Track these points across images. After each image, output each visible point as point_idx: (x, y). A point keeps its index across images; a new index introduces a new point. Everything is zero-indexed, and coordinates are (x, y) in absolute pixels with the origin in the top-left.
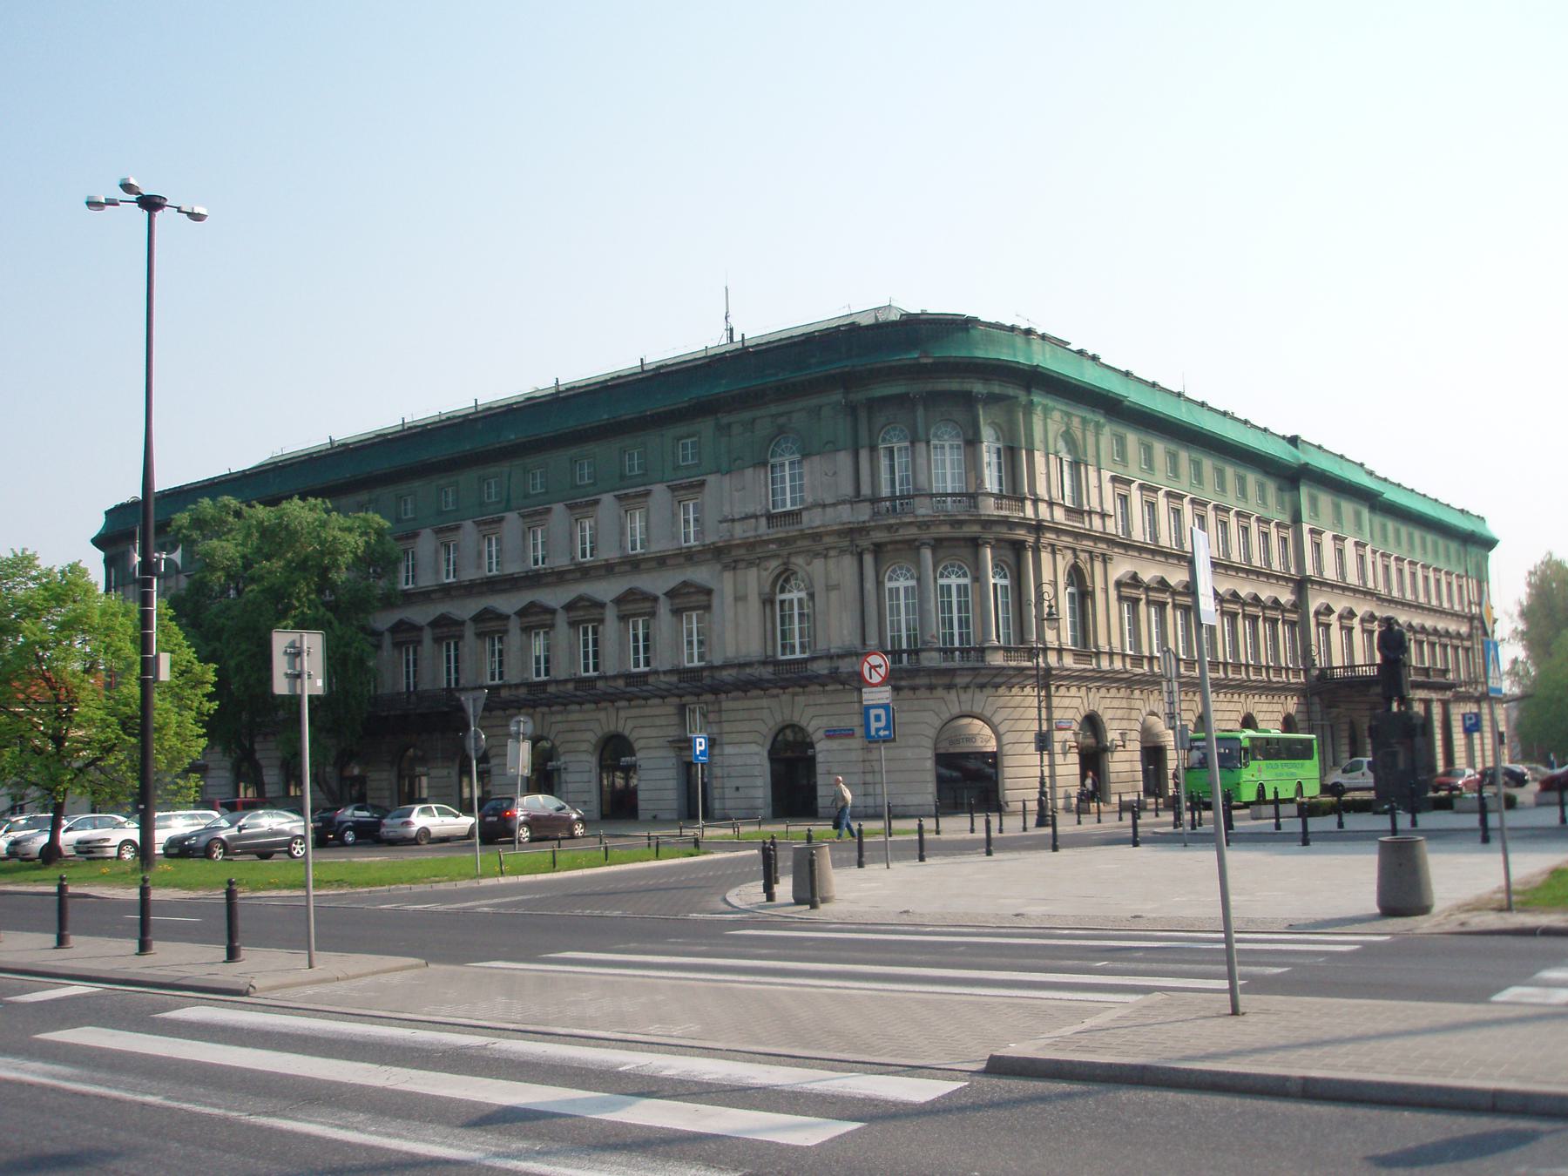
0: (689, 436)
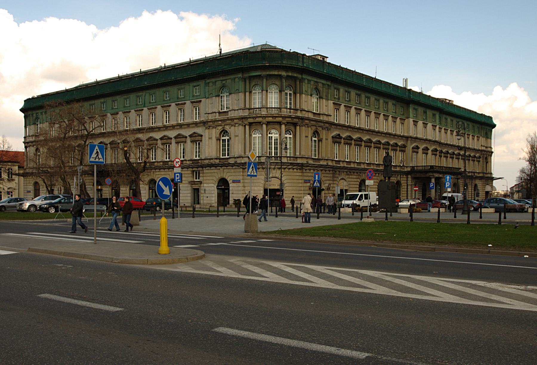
0: (197, 86)
